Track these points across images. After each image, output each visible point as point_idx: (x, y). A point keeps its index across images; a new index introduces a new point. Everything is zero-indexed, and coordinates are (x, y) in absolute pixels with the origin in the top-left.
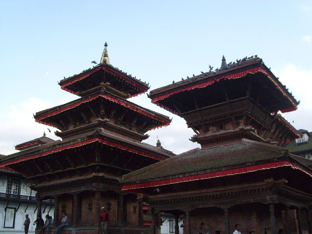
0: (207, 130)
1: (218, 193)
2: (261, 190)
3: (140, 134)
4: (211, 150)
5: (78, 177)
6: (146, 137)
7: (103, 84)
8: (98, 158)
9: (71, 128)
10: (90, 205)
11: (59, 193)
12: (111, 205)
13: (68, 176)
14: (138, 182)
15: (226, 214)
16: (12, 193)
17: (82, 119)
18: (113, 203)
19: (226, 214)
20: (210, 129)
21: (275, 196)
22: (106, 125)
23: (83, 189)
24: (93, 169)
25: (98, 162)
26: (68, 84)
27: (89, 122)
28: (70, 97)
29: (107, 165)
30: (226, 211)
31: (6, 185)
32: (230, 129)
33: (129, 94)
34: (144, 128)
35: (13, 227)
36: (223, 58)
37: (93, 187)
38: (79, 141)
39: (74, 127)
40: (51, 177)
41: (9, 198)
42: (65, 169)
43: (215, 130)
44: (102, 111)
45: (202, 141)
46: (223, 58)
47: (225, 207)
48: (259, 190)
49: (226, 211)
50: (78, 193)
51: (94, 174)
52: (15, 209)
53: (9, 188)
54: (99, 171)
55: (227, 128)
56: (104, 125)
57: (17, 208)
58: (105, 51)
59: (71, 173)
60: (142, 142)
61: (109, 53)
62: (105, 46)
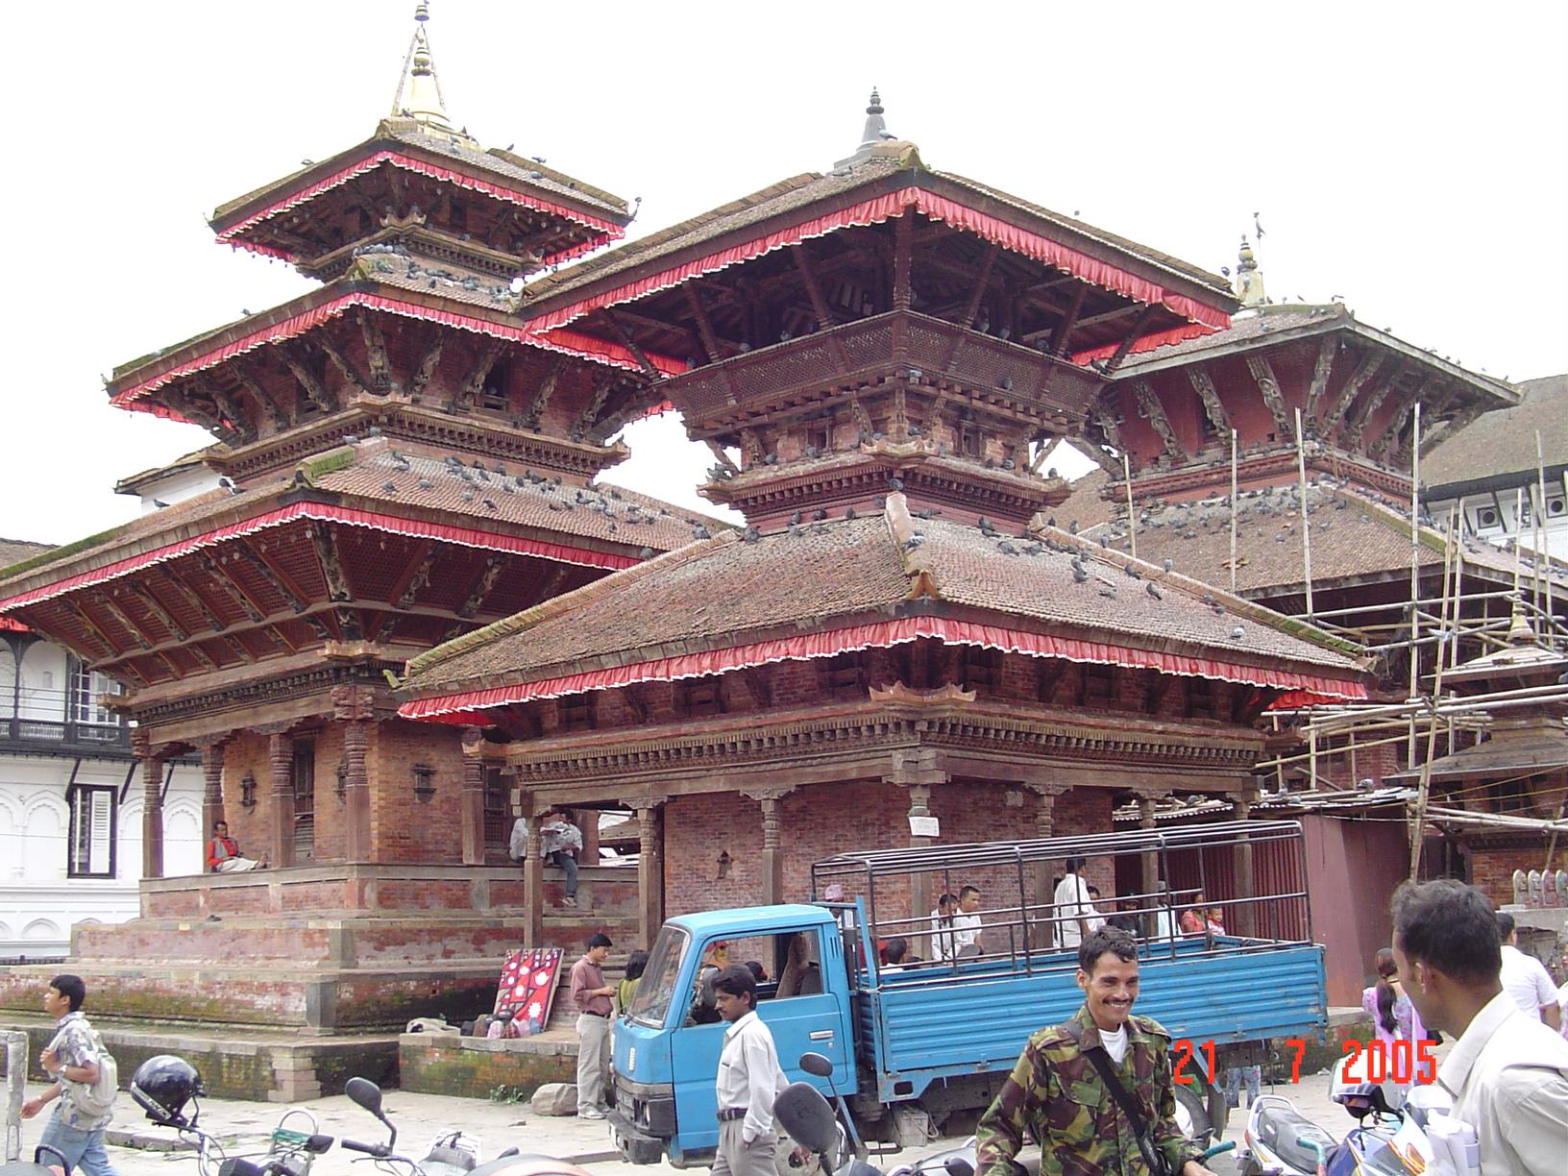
0: (764, 453)
1: (737, 737)
2: (878, 730)
3: (585, 446)
4: (786, 545)
5: (281, 660)
6: (615, 458)
7: (395, 221)
8: (335, 580)
9: (270, 436)
10: (249, 786)
11: (219, 725)
12: (433, 773)
13: (245, 657)
14: (456, 687)
15: (769, 825)
16: (92, 720)
17: (302, 393)
18: (442, 767)
19: (769, 825)
20: (779, 445)
21: (929, 754)
22: (401, 422)
23: (302, 709)
24: (328, 626)
25: (341, 597)
26: (263, 224)
27: (337, 407)
28: (276, 283)
29: (386, 607)
30: (768, 808)
31: (60, 682)
32: (850, 453)
33: (533, 258)
34: (605, 413)
35: (111, 874)
36: (875, 99)
37: (328, 703)
38: (259, 504)
39: (280, 430)
40: (183, 662)
41: (77, 741)
42: (121, 652)
43: (796, 453)
44: (377, 361)
45: (745, 501)
46: (875, 99)
47: (764, 794)
48: (871, 728)
49: (768, 808)
50: (285, 729)
51: (329, 649)
52: (113, 789)
53: (75, 696)
54: (352, 634)
55: (842, 444)
56: (390, 420)
57: (121, 786)
58: (417, 44)
59: (255, 644)
60: (596, 481)
61: (437, 59)
62: (417, 18)
